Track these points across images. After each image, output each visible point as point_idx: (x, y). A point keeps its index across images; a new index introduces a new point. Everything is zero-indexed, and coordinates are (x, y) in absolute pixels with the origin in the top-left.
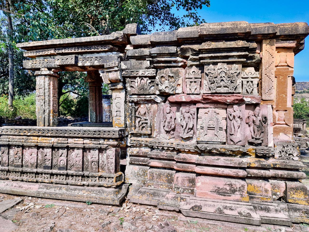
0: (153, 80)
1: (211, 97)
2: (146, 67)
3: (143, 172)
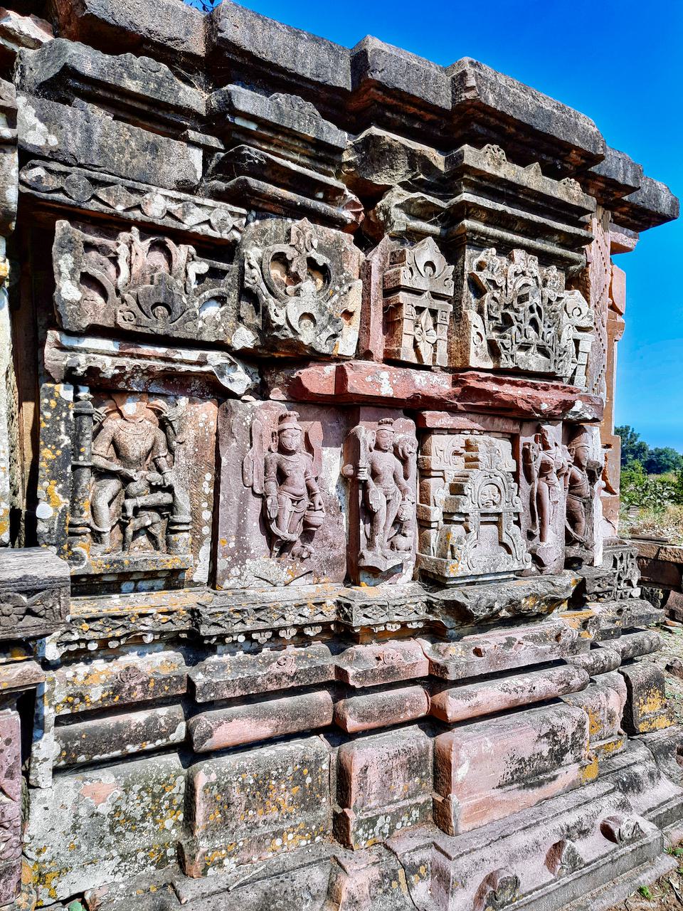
0: (223, 265)
1: (493, 387)
2: (180, 177)
3: (148, 799)
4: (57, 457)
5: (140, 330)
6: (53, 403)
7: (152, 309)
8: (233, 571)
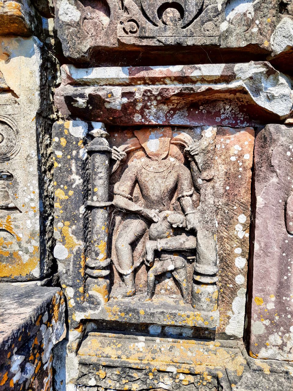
4: (70, 197)
5: (145, 42)
6: (63, 142)
7: (160, 16)
8: (272, 338)
